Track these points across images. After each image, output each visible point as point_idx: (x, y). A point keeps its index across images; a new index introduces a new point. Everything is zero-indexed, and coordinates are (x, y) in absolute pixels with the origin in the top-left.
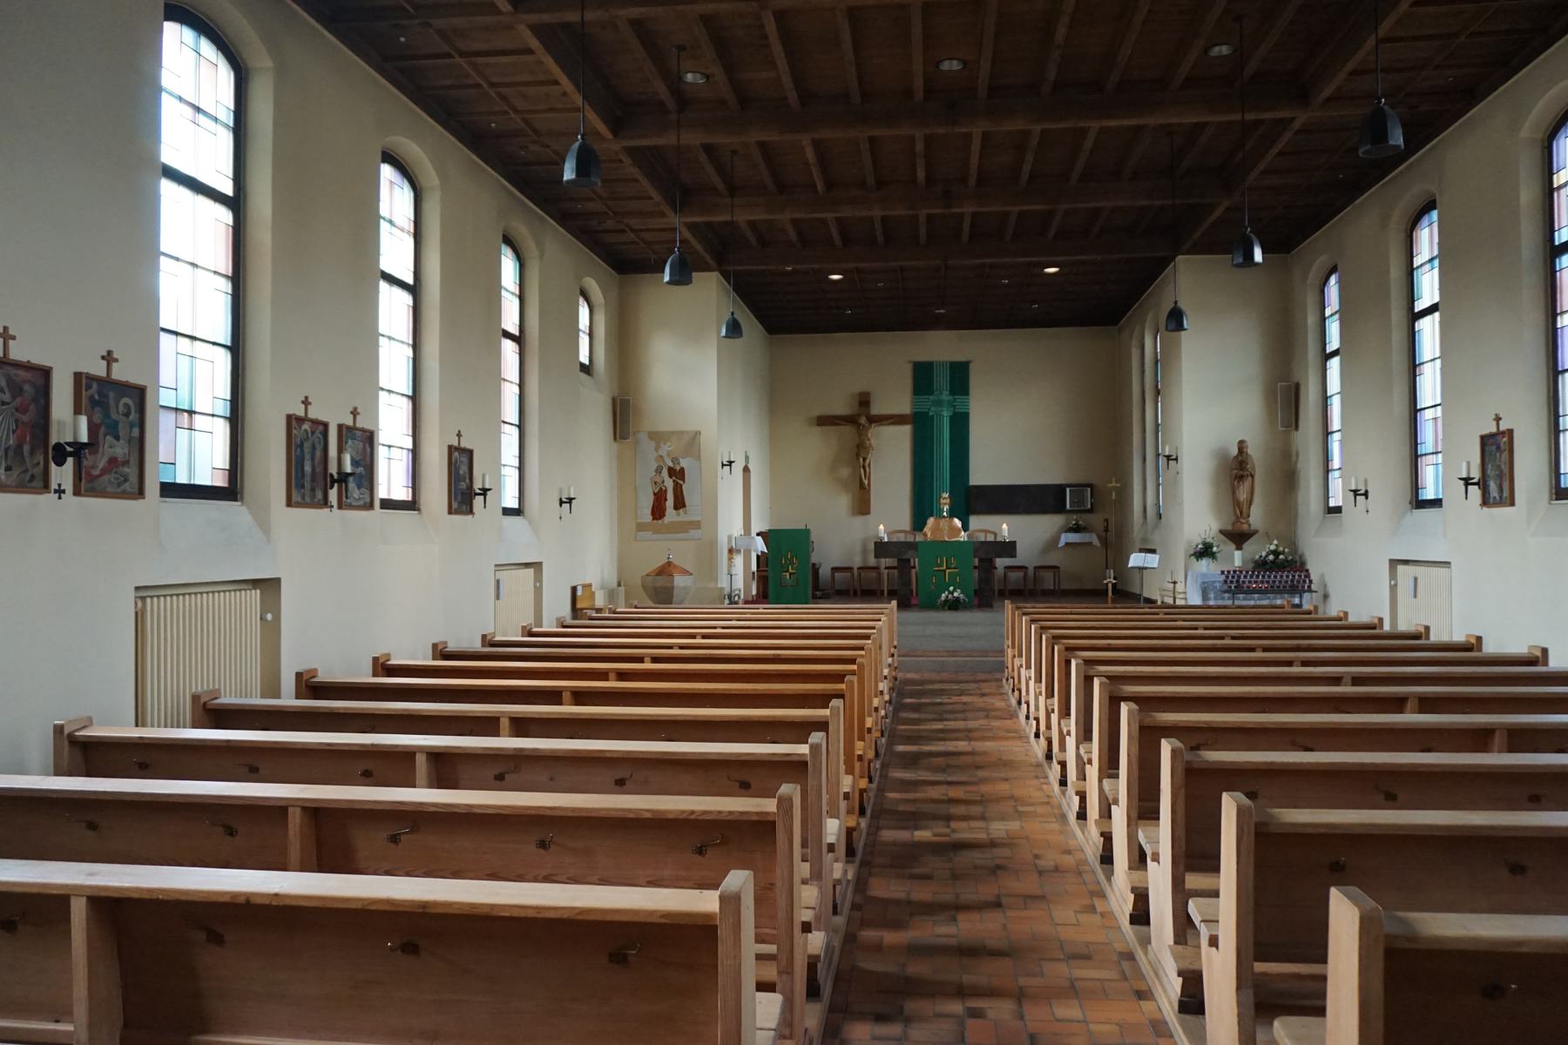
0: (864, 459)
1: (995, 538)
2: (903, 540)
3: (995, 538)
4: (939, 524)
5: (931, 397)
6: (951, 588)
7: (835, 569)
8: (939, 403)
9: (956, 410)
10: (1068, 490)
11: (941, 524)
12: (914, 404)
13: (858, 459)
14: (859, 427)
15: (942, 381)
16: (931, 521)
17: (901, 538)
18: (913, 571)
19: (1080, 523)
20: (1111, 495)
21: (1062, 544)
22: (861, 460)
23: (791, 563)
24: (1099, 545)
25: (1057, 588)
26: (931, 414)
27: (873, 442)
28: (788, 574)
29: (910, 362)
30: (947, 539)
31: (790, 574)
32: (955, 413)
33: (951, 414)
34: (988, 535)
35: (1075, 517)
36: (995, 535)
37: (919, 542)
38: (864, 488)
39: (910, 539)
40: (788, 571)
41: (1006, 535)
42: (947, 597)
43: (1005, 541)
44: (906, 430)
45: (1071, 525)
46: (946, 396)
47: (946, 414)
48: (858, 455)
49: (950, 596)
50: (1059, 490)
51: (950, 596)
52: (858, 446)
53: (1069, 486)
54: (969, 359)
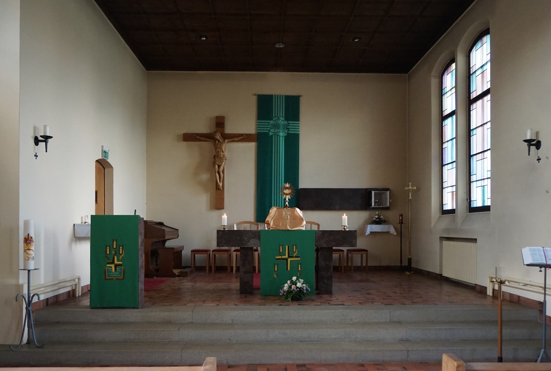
0: (219, 166)
1: (319, 228)
2: (248, 229)
3: (319, 228)
4: (282, 214)
5: (271, 122)
6: (294, 278)
7: (194, 252)
8: (277, 126)
9: (289, 132)
10: (373, 192)
11: (284, 213)
12: (258, 126)
13: (214, 166)
14: (215, 142)
15: (279, 111)
16: (273, 211)
17: (247, 227)
18: (256, 254)
19: (382, 217)
20: (409, 197)
21: (368, 232)
22: (217, 166)
23: (117, 253)
24: (395, 234)
25: (364, 264)
26: (271, 134)
27: (226, 154)
28: (113, 266)
29: (255, 95)
30: (290, 229)
31: (116, 266)
32: (288, 134)
33: (286, 134)
34: (313, 225)
35: (377, 213)
36: (318, 225)
37: (260, 231)
38: (219, 189)
39: (254, 228)
40: (113, 263)
41: (346, 225)
42: (290, 287)
43: (345, 231)
44: (252, 146)
45: (374, 219)
46: (282, 121)
47: (282, 134)
48: (214, 163)
49: (293, 287)
50: (367, 193)
51: (293, 287)
52: (215, 157)
53: (374, 189)
54: (300, 94)
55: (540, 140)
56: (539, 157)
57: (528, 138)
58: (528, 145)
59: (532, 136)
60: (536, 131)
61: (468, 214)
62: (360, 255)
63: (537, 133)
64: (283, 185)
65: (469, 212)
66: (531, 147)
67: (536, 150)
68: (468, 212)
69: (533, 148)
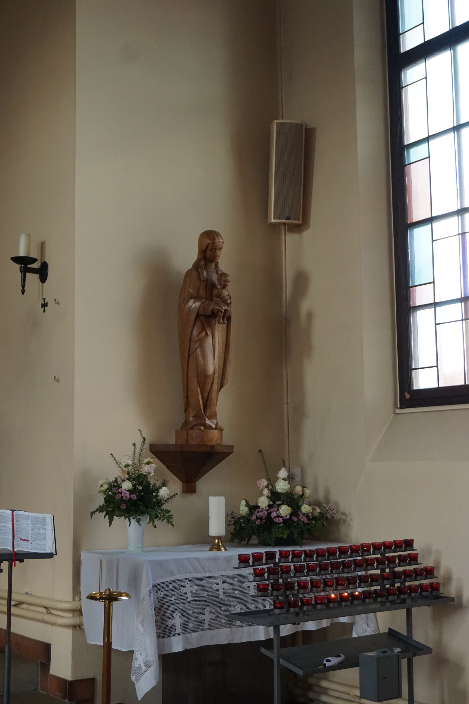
55: (46, 260)
56: (44, 299)
57: (22, 253)
58: (21, 271)
59: (29, 252)
60: (41, 241)
61: (398, 411)
62: (405, 610)
63: (42, 245)
64: (34, 542)
65: (401, 408)
66: (28, 275)
67: (41, 283)
68: (399, 406)
69: (32, 278)
